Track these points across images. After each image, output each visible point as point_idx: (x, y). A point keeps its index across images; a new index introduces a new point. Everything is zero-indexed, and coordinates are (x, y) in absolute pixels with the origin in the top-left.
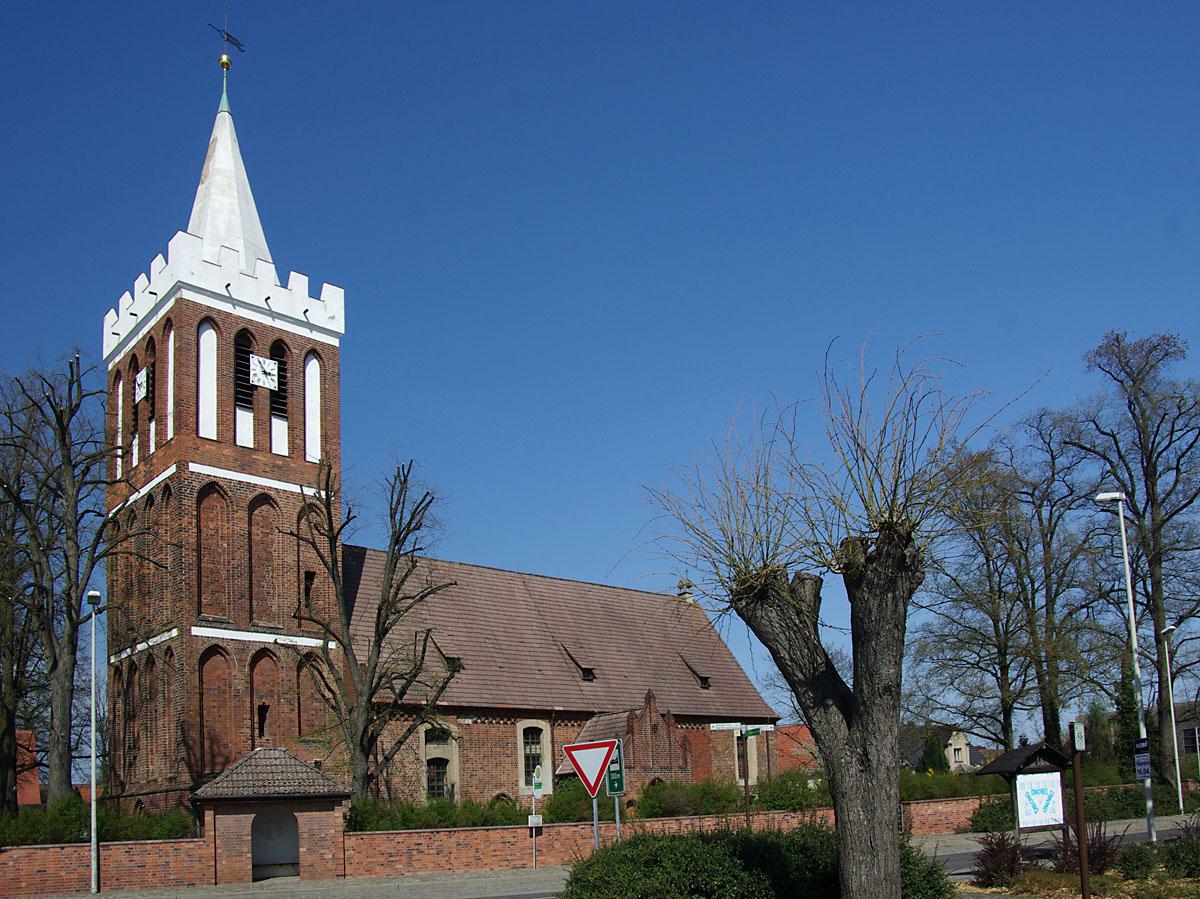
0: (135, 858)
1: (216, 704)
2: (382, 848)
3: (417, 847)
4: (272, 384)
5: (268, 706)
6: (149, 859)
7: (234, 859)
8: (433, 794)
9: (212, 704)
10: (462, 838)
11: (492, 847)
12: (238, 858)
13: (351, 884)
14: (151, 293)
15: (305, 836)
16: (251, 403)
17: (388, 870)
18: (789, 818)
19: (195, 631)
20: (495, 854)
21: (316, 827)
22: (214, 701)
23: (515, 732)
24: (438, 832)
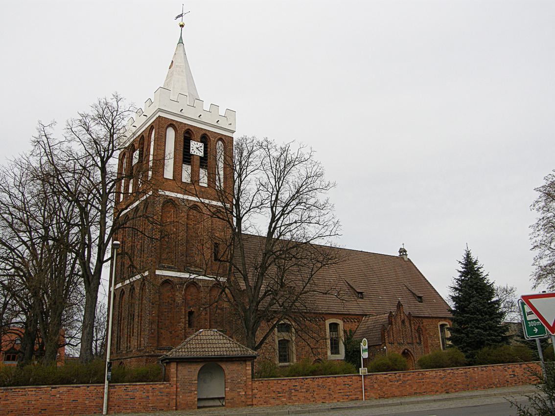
0: (130, 393)
1: (166, 310)
2: (274, 389)
3: (294, 387)
4: (201, 154)
5: (194, 312)
6: (138, 394)
7: (187, 395)
8: (284, 357)
9: (165, 310)
10: (321, 382)
11: (338, 387)
12: (189, 394)
13: (256, 409)
15: (229, 381)
16: (190, 162)
17: (278, 402)
18: (506, 368)
19: (158, 272)
20: (339, 391)
21: (235, 375)
22: (165, 309)
23: (325, 326)
24: (306, 379)
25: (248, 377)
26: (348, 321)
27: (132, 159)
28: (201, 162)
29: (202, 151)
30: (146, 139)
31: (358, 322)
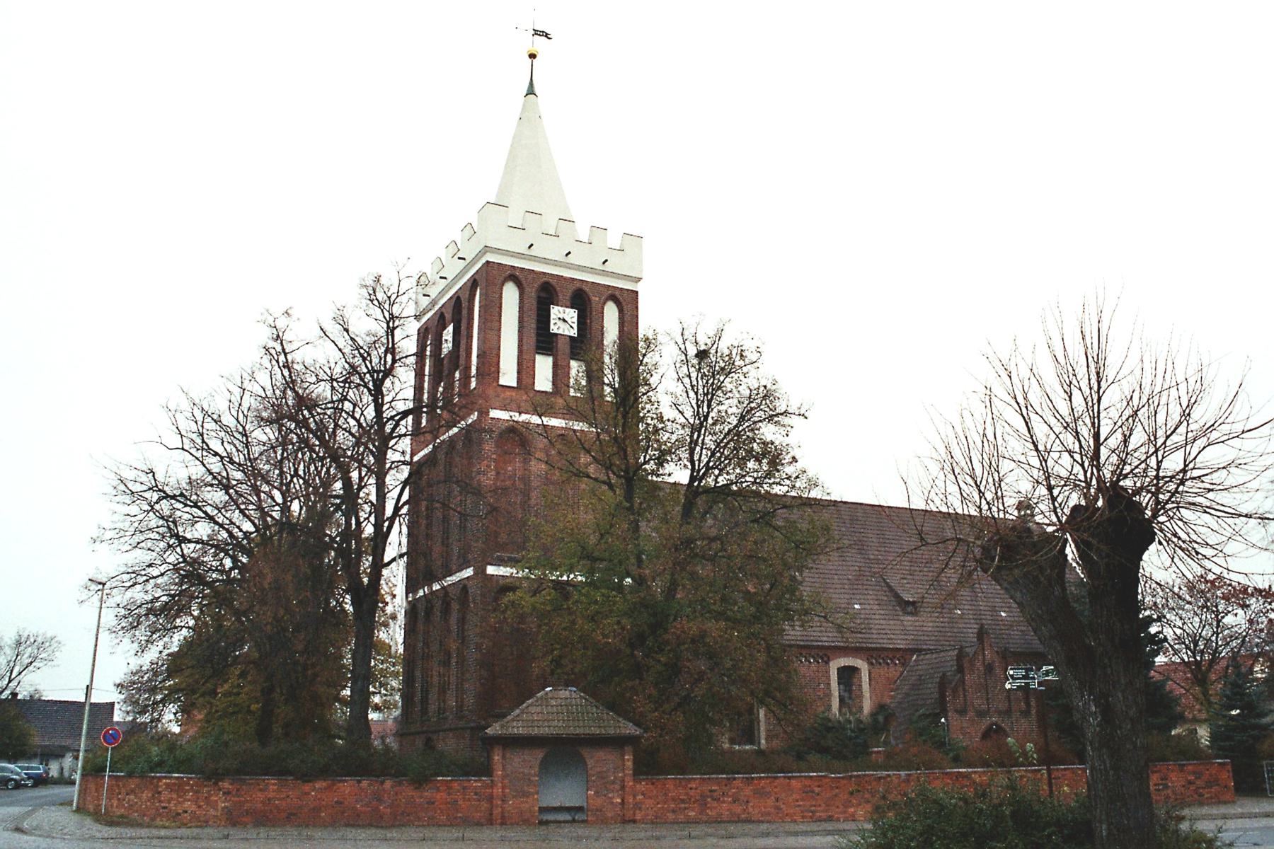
4: (573, 332)
14: (459, 258)
19: (491, 570)
23: (828, 672)
25: (627, 772)
26: (880, 664)
27: (441, 344)
28: (572, 348)
29: (575, 326)
30: (465, 304)
31: (903, 664)
